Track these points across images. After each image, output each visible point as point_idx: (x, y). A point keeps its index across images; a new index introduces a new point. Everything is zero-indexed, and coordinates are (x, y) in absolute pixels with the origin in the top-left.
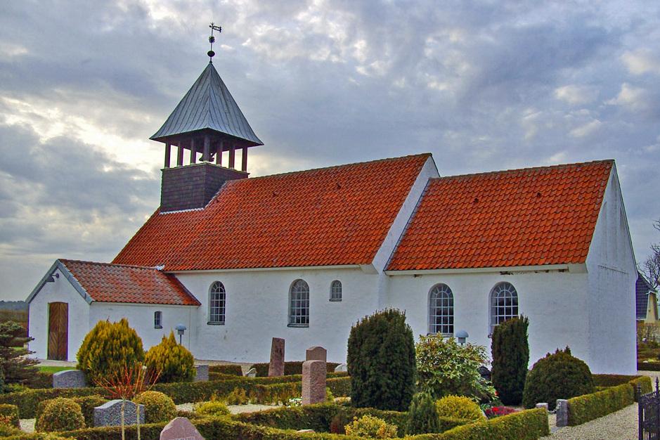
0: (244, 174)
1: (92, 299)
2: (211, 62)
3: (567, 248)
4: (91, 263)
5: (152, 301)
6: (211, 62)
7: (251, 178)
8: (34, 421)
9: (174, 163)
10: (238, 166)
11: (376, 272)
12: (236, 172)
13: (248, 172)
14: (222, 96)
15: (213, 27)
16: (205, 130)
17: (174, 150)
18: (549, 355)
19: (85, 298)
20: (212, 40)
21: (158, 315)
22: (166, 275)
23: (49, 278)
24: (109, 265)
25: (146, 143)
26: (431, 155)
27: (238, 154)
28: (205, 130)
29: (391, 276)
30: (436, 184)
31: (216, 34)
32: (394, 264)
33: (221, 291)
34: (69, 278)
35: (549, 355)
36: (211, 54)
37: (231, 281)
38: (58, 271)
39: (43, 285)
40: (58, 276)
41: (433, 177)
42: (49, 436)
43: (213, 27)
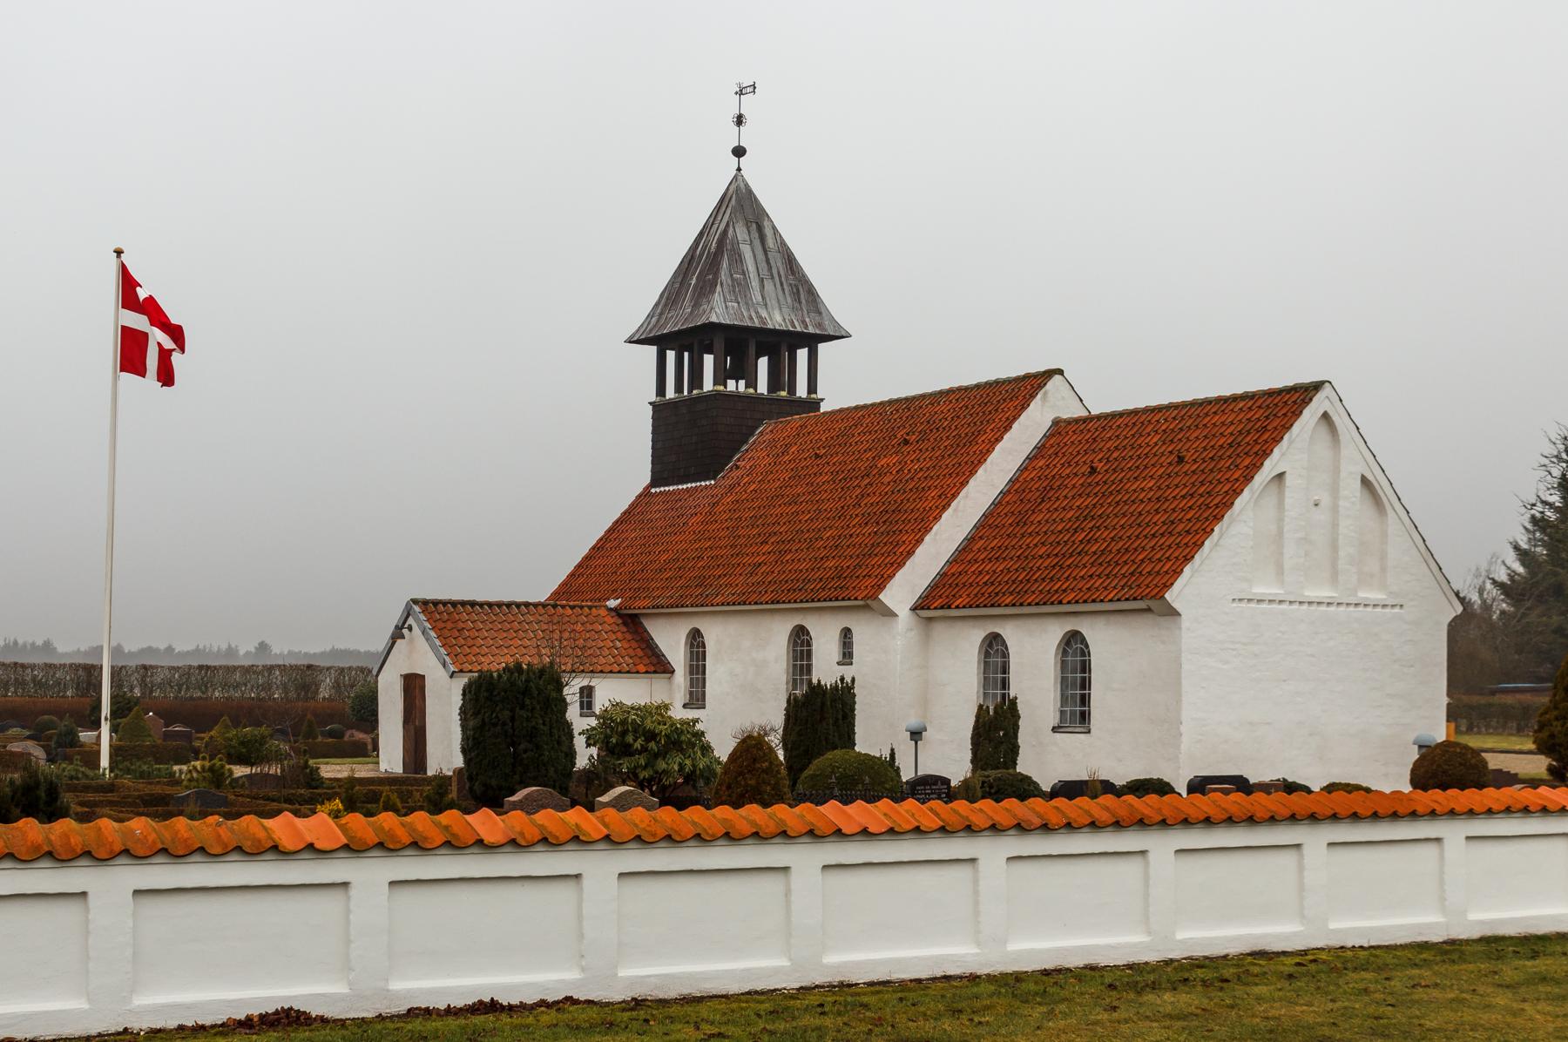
0: (814, 405)
1: (452, 668)
2: (739, 169)
4: (473, 604)
5: (608, 668)
6: (739, 169)
7: (833, 413)
11: (890, 614)
12: (801, 401)
13: (820, 396)
14: (757, 243)
17: (671, 356)
19: (444, 665)
22: (620, 616)
24: (544, 605)
25: (190, 647)
26: (1060, 372)
29: (930, 619)
32: (939, 601)
33: (1083, 654)
36: (739, 152)
37: (716, 633)
38: (411, 621)
39: (393, 644)
40: (410, 628)
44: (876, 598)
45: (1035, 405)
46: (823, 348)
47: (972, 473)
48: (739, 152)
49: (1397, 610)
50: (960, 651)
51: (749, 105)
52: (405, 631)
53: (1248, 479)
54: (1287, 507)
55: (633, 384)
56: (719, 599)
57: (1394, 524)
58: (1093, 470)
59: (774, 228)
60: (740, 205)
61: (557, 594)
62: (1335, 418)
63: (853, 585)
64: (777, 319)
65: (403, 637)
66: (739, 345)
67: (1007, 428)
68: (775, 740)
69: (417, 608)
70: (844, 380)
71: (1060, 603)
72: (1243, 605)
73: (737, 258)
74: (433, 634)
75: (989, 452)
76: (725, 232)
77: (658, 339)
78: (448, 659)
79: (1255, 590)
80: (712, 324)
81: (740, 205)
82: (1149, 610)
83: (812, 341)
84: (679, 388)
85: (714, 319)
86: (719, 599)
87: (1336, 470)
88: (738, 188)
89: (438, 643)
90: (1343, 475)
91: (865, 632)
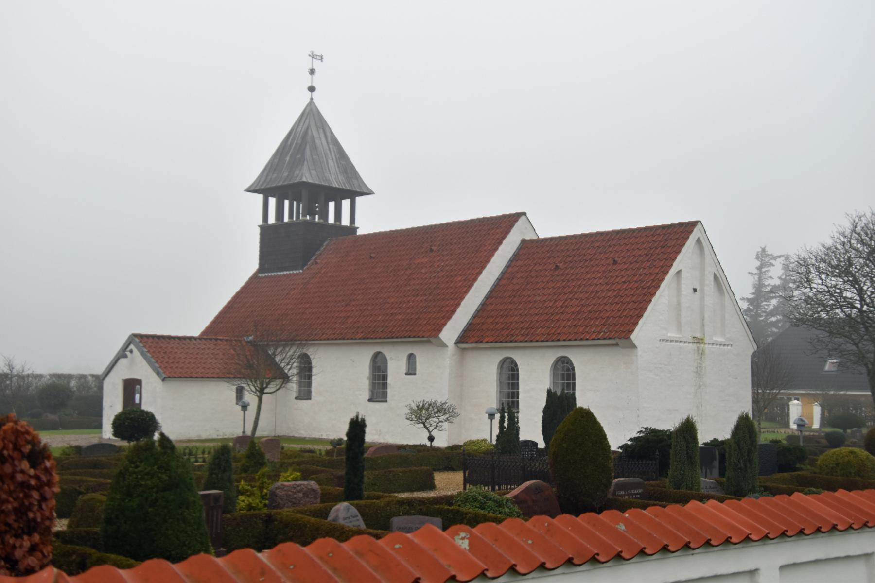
0: (352, 229)
1: (164, 376)
2: (312, 99)
3: (614, 324)
6: (312, 99)
7: (365, 236)
8: (468, 548)
9: (272, 220)
10: (345, 221)
11: (444, 345)
15: (313, 56)
16: (306, 183)
18: (688, 429)
20: (312, 72)
21: (411, 358)
23: (122, 354)
26: (525, 214)
27: (346, 204)
28: (306, 183)
29: (464, 349)
30: (532, 249)
31: (317, 64)
32: (471, 337)
34: (142, 354)
35: (688, 429)
36: (312, 89)
38: (132, 347)
40: (131, 351)
41: (528, 238)
42: (2, 433)
43: (313, 56)
44: (437, 336)
45: (514, 231)
46: (358, 199)
47: (484, 267)
48: (312, 89)
49: (729, 348)
50: (486, 368)
51: (317, 64)
52: (128, 353)
53: (665, 273)
54: (683, 289)
55: (250, 215)
56: (324, 336)
57: (728, 302)
58: (557, 267)
59: (332, 132)
60: (311, 118)
61: (205, 333)
62: (703, 241)
63: (422, 329)
64: (336, 180)
65: (125, 356)
66: (316, 196)
67: (500, 243)
68: (750, 415)
69: (137, 340)
70: (371, 218)
71: (558, 340)
72: (664, 343)
73: (314, 147)
74: (149, 355)
75: (492, 255)
76: (306, 132)
77: (264, 188)
78: (160, 370)
79: (669, 335)
80: (304, 183)
81: (311, 118)
82: (617, 345)
83: (352, 195)
84: (298, 216)
85: (304, 179)
86: (324, 336)
87: (702, 269)
88: (311, 110)
89: (153, 360)
90: (706, 272)
91: (424, 356)
